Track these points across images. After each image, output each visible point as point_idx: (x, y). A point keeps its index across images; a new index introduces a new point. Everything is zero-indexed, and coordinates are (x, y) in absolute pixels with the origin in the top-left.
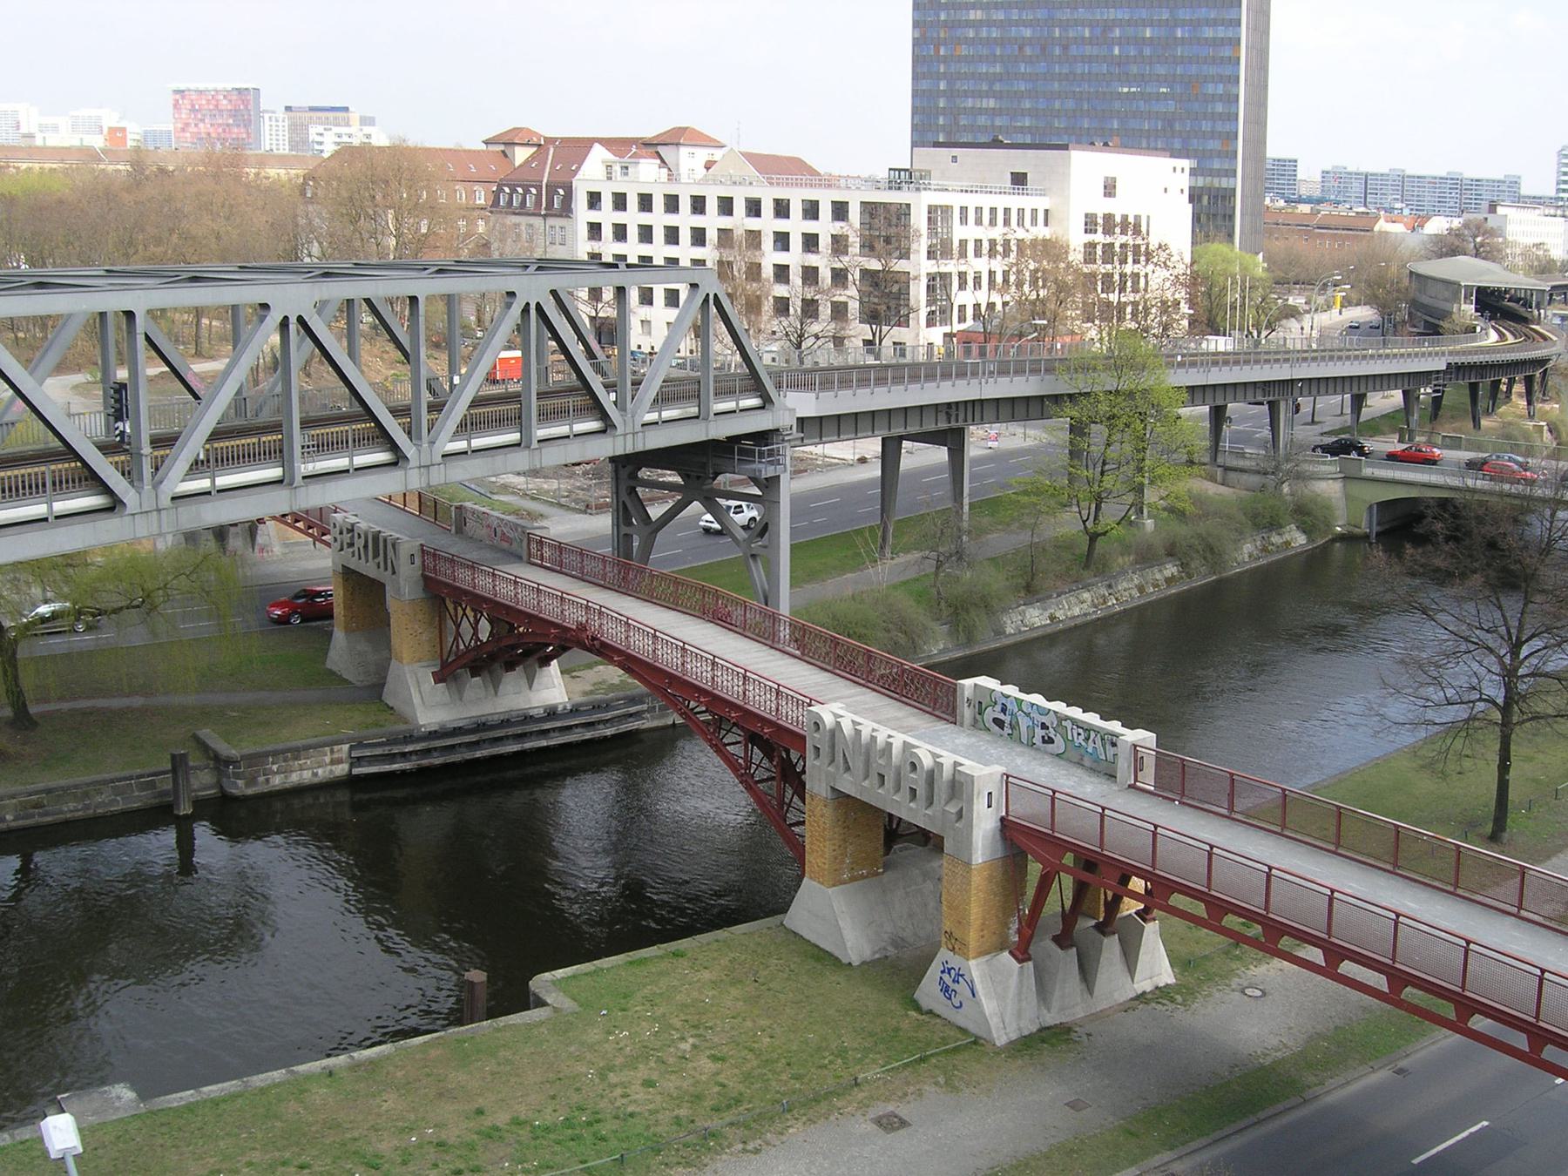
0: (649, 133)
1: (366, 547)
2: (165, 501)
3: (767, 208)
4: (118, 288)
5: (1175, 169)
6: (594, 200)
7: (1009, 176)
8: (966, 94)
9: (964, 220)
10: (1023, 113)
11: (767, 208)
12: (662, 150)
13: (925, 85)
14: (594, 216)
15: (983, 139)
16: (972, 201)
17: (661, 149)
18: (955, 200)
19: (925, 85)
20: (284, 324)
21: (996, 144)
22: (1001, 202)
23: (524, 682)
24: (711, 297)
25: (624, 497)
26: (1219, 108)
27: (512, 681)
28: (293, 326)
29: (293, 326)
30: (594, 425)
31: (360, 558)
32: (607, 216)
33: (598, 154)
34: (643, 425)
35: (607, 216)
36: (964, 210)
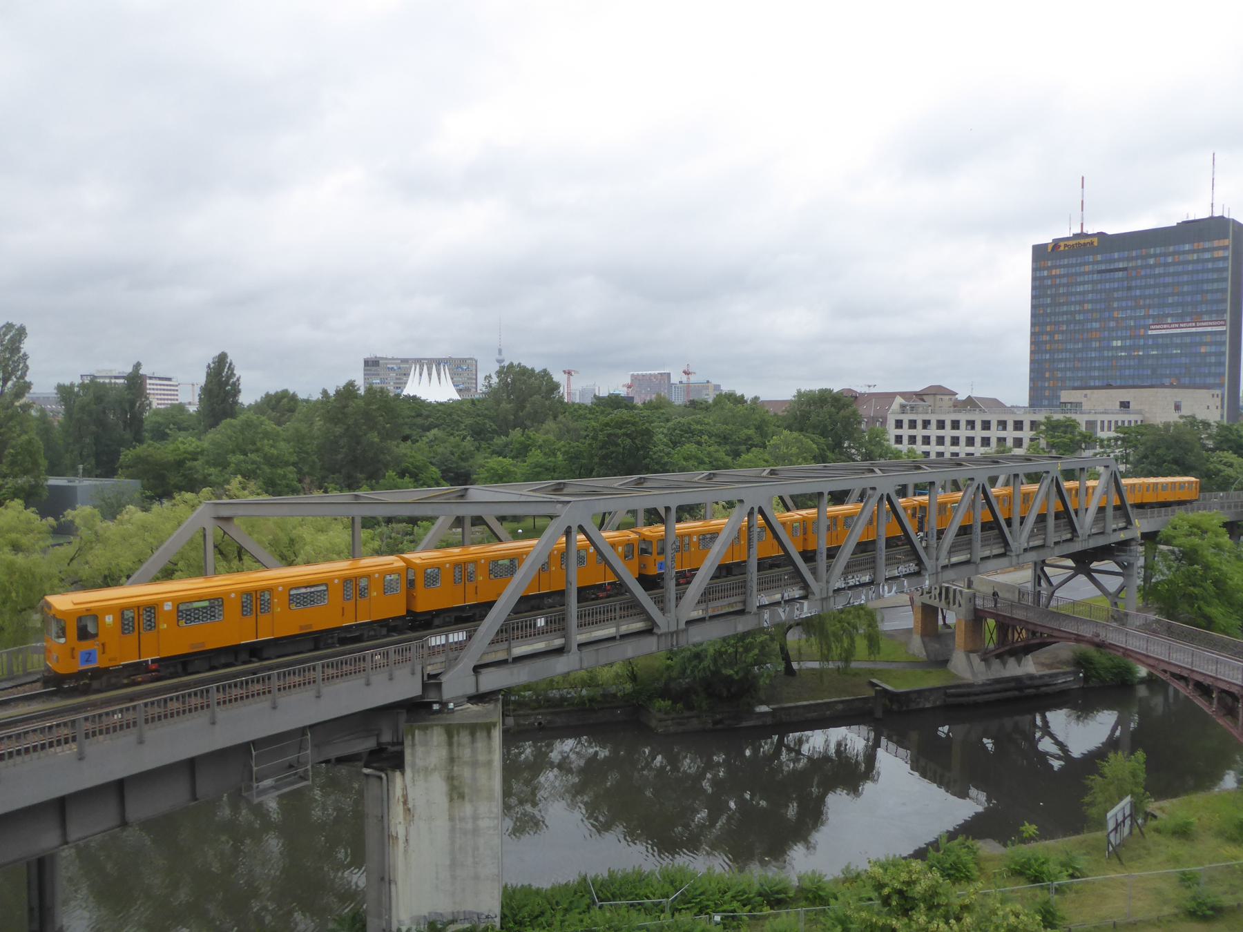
0: (918, 389)
1: (940, 594)
2: (831, 593)
3: (948, 424)
4: (656, 492)
5: (1213, 396)
6: (899, 424)
7: (1118, 403)
8: (1061, 360)
9: (1102, 429)
10: (1095, 368)
11: (948, 424)
12: (925, 397)
13: (1036, 357)
14: (899, 432)
15: (1077, 384)
16: (1106, 418)
17: (925, 397)
18: (1099, 418)
19: (1036, 357)
20: (881, 498)
21: (1109, 387)
22: (1113, 418)
23: (1017, 666)
24: (756, 510)
25: (1039, 572)
26: (1213, 359)
27: (1012, 662)
28: (885, 499)
29: (885, 499)
30: (638, 626)
31: (935, 599)
32: (905, 432)
33: (899, 400)
34: (835, 591)
35: (905, 432)
36: (1103, 422)
